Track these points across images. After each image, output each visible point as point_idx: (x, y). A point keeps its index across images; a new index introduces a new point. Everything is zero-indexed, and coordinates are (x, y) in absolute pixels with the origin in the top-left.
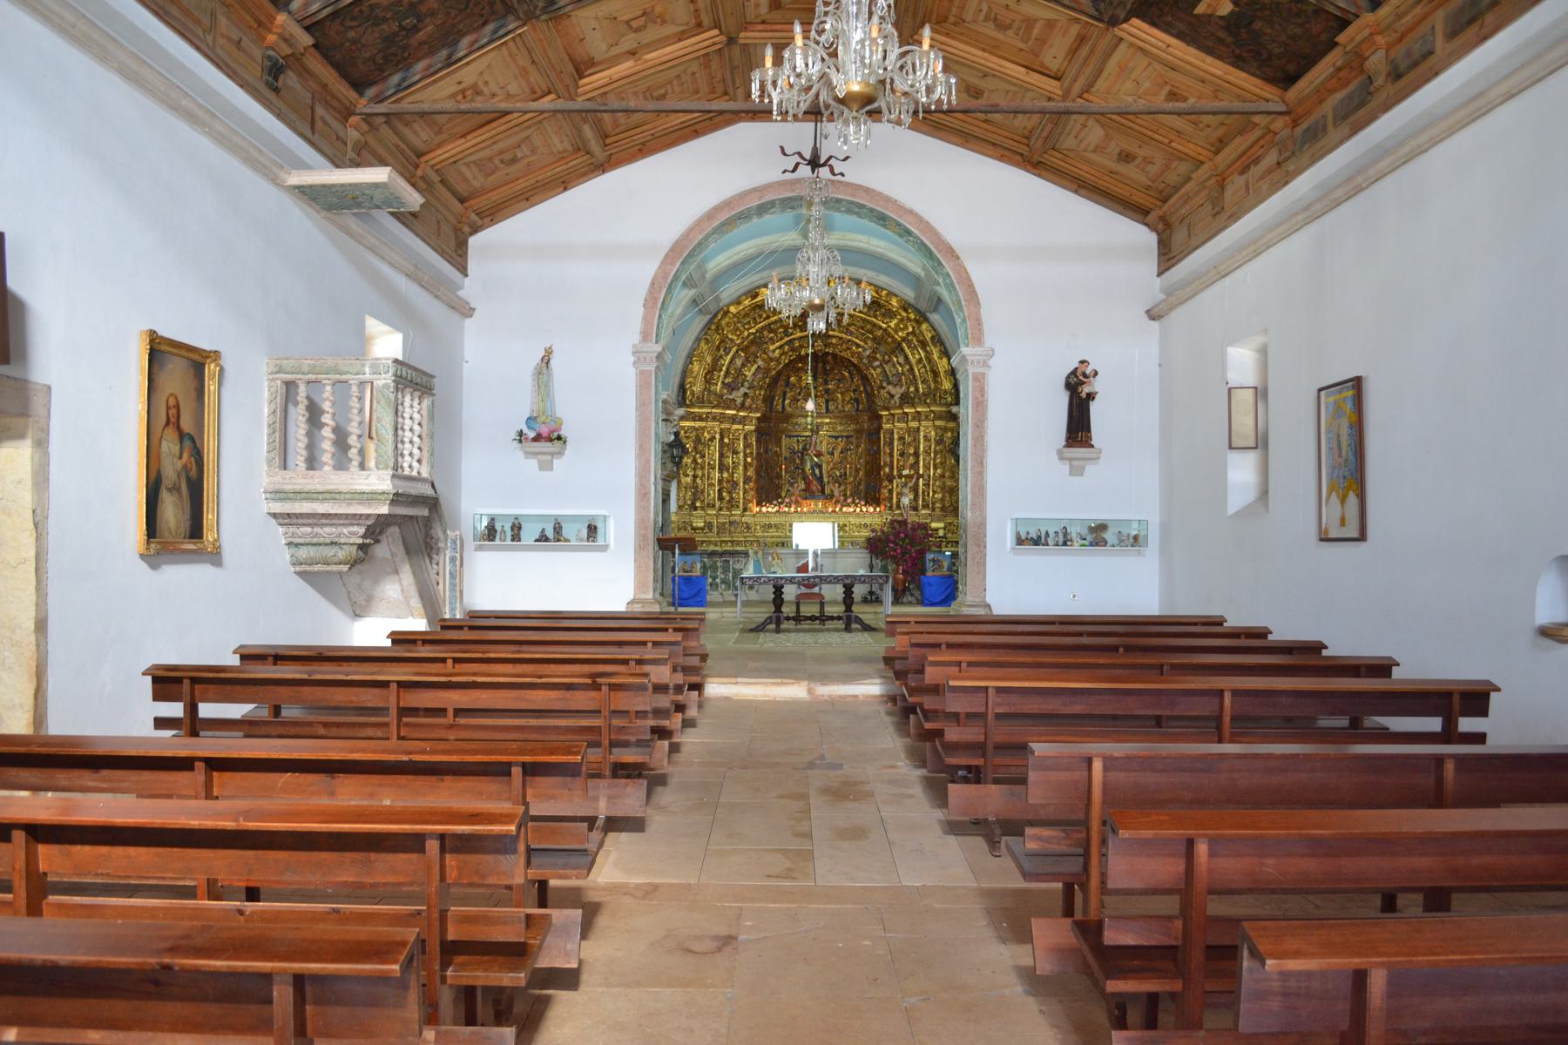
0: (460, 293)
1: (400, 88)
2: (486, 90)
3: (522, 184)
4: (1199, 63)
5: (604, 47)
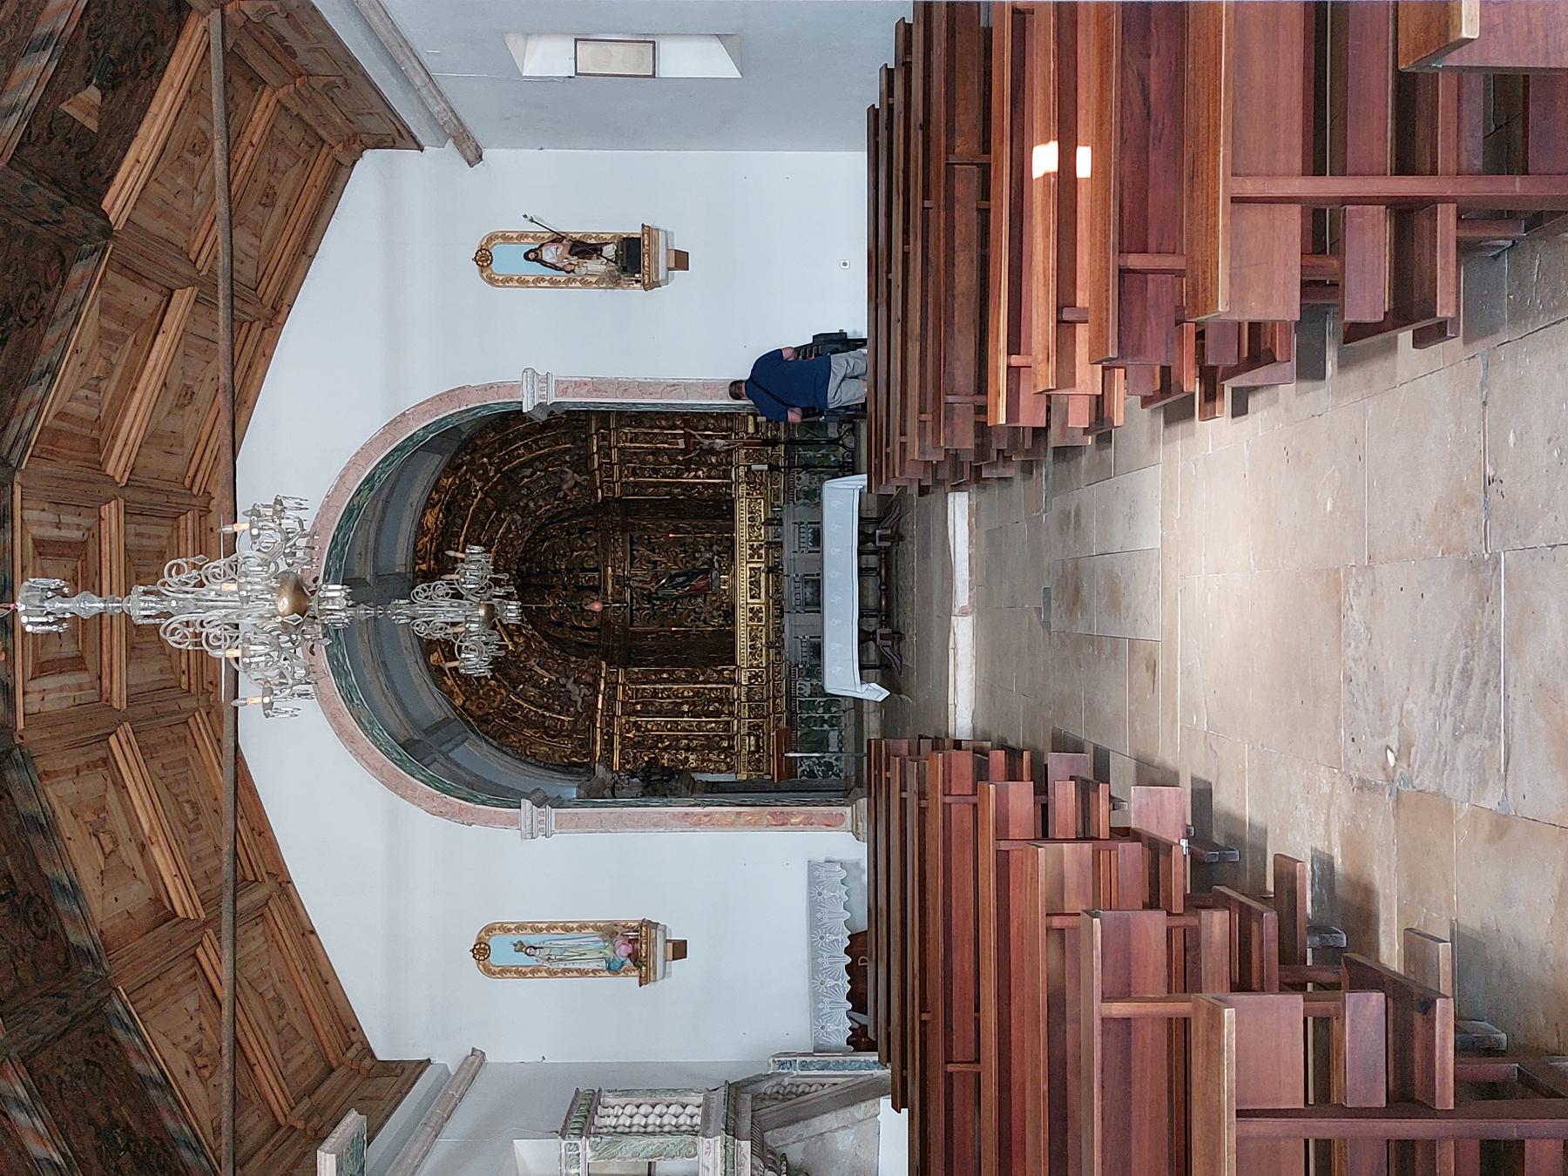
0: (452, 1070)
1: (198, 1150)
2: (197, 1038)
3: (309, 991)
4: (159, 121)
5: (137, 886)
